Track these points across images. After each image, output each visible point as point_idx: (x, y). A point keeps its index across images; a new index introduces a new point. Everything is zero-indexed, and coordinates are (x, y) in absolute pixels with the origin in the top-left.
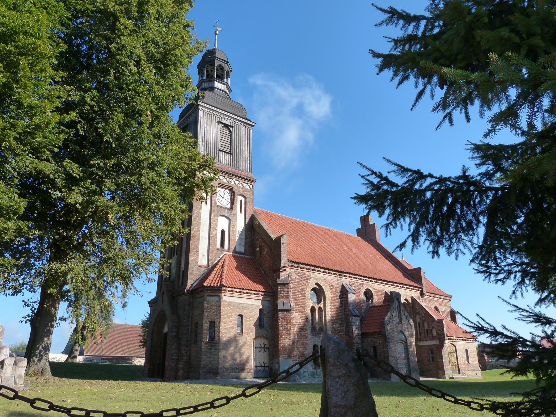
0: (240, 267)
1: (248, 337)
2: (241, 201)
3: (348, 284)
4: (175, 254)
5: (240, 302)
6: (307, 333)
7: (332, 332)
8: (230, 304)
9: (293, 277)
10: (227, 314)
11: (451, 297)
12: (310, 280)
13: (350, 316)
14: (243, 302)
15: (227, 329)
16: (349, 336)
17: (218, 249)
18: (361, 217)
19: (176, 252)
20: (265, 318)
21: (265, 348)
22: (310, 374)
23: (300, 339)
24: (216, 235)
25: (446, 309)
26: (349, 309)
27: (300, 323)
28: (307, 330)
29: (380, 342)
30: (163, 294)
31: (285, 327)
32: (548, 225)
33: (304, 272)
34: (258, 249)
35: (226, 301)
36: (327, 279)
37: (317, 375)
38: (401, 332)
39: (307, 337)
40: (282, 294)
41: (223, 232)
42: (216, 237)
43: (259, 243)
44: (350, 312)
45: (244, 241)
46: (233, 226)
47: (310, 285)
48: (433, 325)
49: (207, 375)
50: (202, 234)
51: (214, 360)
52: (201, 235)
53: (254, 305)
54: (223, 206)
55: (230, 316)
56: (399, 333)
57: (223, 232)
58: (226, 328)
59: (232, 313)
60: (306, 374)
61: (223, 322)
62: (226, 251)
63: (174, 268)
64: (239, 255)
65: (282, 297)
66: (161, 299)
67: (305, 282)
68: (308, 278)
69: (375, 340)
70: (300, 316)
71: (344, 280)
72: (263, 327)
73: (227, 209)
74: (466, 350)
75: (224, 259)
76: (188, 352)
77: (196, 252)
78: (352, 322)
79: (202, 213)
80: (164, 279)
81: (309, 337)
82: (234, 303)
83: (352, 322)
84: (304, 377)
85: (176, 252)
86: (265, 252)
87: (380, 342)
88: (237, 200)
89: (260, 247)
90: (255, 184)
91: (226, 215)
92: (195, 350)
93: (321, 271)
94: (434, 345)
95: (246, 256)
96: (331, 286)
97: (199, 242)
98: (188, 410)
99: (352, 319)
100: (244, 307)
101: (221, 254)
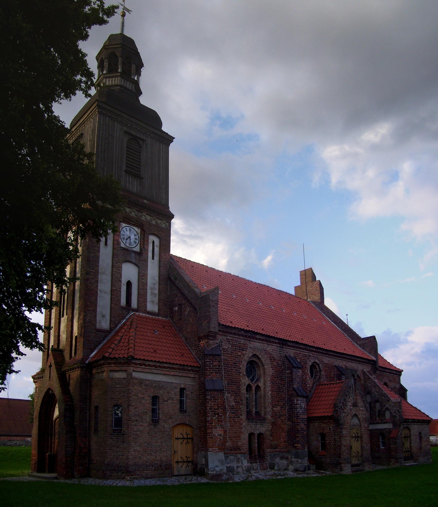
0: (153, 332)
1: (166, 426)
2: (153, 242)
4: (65, 314)
5: (156, 379)
6: (242, 419)
7: (272, 417)
8: (141, 382)
9: (225, 347)
10: (137, 396)
12: (246, 351)
13: (295, 397)
14: (159, 380)
15: (138, 415)
16: (292, 421)
17: (122, 308)
18: (300, 272)
19: (65, 311)
20: (188, 401)
21: (187, 438)
22: (244, 469)
23: (233, 426)
24: (120, 288)
25: (395, 385)
26: (293, 388)
27: (233, 406)
28: (241, 415)
29: (330, 429)
30: (50, 366)
33: (239, 340)
34: (176, 308)
35: (136, 379)
36: (268, 349)
37: (253, 469)
38: (356, 415)
39: (242, 424)
40: (211, 368)
41: (129, 284)
42: (120, 291)
43: (178, 300)
44: (295, 391)
45: (157, 296)
46: (143, 276)
47: (245, 358)
48: (387, 406)
50: (101, 286)
51: (123, 456)
52: (99, 288)
53: (173, 383)
54: (130, 249)
56: (353, 417)
57: (129, 284)
58: (137, 414)
59: (144, 394)
60: (240, 469)
61: (132, 406)
62: (134, 310)
63: (64, 333)
64: (151, 316)
65: (212, 373)
66: (48, 374)
67: (239, 354)
68: (243, 349)
69: (323, 425)
70: (233, 397)
72: (185, 412)
73: (135, 252)
74: (420, 433)
75: (130, 320)
76: (87, 443)
77: (94, 311)
78: (297, 404)
79: (101, 258)
80: (51, 347)
81: (244, 424)
82: (146, 380)
84: (238, 473)
85: (65, 311)
86: (187, 313)
87: (330, 429)
88: (148, 241)
89: (180, 305)
91: (133, 261)
92: (95, 442)
93: (260, 339)
94: (386, 429)
95: (160, 318)
96: (272, 359)
97: (97, 298)
98: (65, 306)
99: (297, 400)
100: (159, 385)
101: (127, 315)
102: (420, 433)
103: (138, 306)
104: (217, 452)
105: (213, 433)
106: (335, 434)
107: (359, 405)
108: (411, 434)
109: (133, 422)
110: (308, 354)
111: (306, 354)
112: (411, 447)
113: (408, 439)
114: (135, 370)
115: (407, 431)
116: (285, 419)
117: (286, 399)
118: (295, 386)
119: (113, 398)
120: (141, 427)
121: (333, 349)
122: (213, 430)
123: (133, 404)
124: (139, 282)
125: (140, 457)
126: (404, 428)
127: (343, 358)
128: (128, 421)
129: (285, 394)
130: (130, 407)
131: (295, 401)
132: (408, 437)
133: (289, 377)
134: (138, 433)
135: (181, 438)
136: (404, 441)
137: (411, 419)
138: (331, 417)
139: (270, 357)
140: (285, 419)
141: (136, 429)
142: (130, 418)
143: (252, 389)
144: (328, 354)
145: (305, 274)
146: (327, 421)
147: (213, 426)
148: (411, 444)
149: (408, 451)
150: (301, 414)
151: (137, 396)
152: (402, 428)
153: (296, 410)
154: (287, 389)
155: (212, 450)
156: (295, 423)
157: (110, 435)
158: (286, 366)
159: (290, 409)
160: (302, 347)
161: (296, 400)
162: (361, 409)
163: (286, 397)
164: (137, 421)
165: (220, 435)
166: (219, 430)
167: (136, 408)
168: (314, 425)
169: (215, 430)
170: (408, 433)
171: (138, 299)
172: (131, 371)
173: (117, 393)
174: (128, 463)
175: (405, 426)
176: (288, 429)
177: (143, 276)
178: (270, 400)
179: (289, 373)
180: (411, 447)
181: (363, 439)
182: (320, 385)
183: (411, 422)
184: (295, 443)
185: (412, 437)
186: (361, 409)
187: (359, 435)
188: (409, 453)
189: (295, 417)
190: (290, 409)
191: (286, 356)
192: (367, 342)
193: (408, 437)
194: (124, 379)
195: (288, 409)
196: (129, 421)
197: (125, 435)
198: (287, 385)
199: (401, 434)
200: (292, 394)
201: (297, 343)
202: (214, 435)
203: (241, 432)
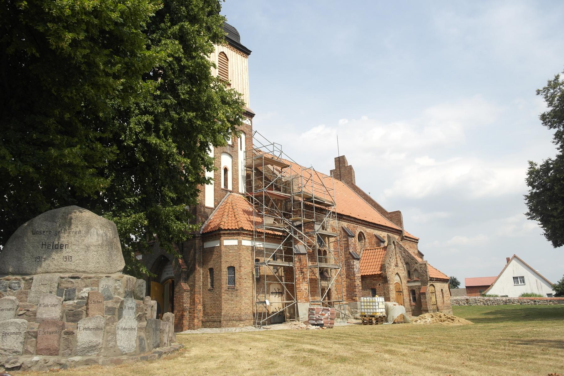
3: (346, 227)
10: (245, 259)
11: (418, 240)
18: (335, 158)
25: (414, 251)
31: (301, 270)
32: (10, 196)
38: (397, 274)
41: (226, 170)
46: (235, 164)
49: (229, 323)
51: (236, 307)
55: (249, 260)
57: (226, 170)
69: (374, 282)
71: (343, 223)
74: (442, 290)
83: (353, 265)
90: (254, 119)
91: (228, 152)
99: (353, 262)
101: (226, 194)
102: (442, 290)
103: (233, 188)
104: (304, 303)
105: (300, 287)
106: (384, 289)
107: (399, 265)
108: (436, 290)
109: (244, 280)
110: (356, 225)
111: (355, 225)
112: (436, 301)
113: (434, 294)
114: (243, 238)
115: (432, 288)
116: (344, 277)
117: (344, 261)
118: (351, 251)
119: (227, 261)
120: (249, 284)
121: (379, 223)
122: (301, 285)
123: (243, 265)
124: (232, 169)
125: (248, 308)
126: (430, 285)
127: (380, 228)
128: (240, 280)
129: (343, 257)
130: (241, 268)
131: (352, 263)
132: (434, 293)
133: (346, 244)
134: (247, 289)
135: (275, 293)
136: (431, 296)
137: (436, 278)
138: (380, 275)
139: (332, 228)
140: (344, 277)
141: (245, 286)
142: (241, 277)
143: (321, 253)
144: (369, 225)
145: (339, 160)
146: (377, 278)
147: (301, 282)
148: (436, 298)
149: (435, 305)
150: (356, 273)
151: (245, 259)
152: (429, 285)
153: (353, 270)
154: (345, 253)
155: (301, 301)
156: (352, 280)
157: (225, 291)
158: (343, 235)
159: (347, 269)
160: (352, 220)
161: (352, 262)
162: (401, 268)
163: (344, 259)
164: (246, 279)
165: (306, 289)
166: (305, 286)
167: (245, 268)
168: (366, 282)
169: (302, 285)
170: (434, 289)
171: (232, 182)
172: (241, 239)
173: (230, 257)
174: (241, 313)
175: (431, 283)
176: (347, 285)
177: (235, 164)
178: (334, 262)
179: (346, 241)
180: (436, 301)
181: (404, 293)
182: (366, 250)
183: (436, 281)
184: (354, 297)
185: (437, 293)
186: (401, 268)
187: (401, 290)
188: (436, 306)
189: (352, 275)
190: (347, 269)
191: (342, 228)
192: (394, 215)
193: (434, 292)
194: (236, 245)
195: (346, 269)
196: (240, 279)
197: (238, 290)
198: (344, 250)
199: (429, 290)
200: (349, 257)
201: (349, 217)
202: (301, 289)
203: (317, 287)
